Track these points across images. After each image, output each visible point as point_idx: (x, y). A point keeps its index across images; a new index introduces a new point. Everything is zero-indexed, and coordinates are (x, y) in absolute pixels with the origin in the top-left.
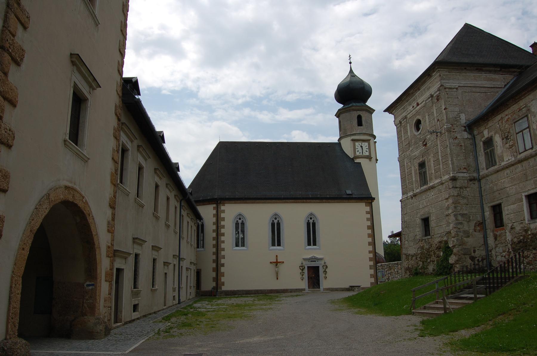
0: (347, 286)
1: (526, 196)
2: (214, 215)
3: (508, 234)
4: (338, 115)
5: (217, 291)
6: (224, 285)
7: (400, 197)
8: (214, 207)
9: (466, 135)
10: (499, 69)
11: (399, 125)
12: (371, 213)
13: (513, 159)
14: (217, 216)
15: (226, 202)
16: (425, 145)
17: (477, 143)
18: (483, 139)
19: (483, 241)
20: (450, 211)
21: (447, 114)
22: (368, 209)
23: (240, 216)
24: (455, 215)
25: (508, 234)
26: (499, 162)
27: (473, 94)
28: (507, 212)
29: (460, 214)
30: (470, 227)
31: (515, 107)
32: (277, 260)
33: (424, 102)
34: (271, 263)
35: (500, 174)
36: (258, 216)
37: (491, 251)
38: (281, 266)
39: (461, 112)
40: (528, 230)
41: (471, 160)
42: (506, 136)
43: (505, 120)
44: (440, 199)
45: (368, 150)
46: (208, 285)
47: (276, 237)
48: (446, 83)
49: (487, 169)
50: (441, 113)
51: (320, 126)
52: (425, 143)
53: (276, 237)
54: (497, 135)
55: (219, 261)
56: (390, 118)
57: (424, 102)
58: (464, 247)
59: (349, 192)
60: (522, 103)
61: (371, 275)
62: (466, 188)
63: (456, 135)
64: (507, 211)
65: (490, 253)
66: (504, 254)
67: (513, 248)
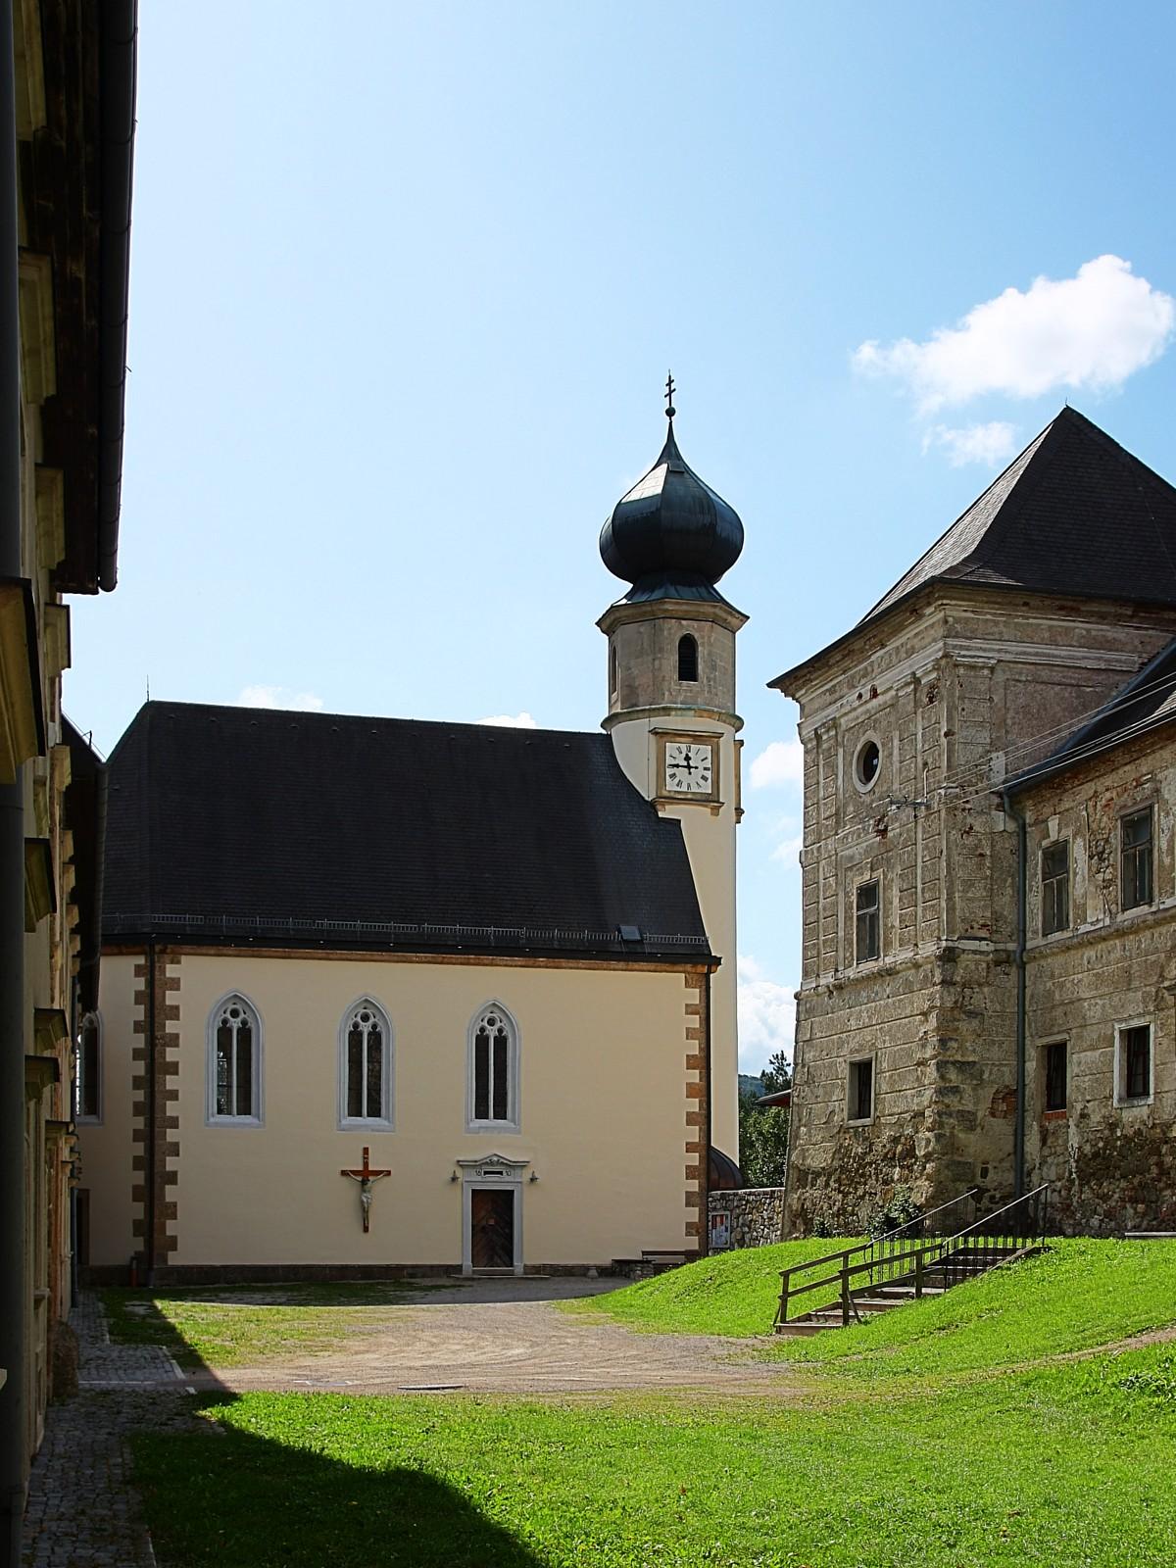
0: (606, 1260)
1: (1121, 1031)
2: (138, 994)
3: (1073, 1130)
4: (610, 623)
5: (150, 1268)
6: (175, 1249)
7: (794, 982)
8: (138, 969)
9: (1001, 821)
10: (1129, 613)
11: (817, 745)
12: (702, 1011)
13: (1107, 922)
14: (150, 999)
15: (187, 948)
16: (883, 833)
17: (1029, 849)
18: (1045, 843)
19: (1012, 1143)
20: (929, 1052)
21: (950, 751)
22: (694, 996)
23: (237, 1005)
24: (940, 1066)
25: (1073, 1130)
26: (1075, 922)
27: (1039, 687)
28: (1076, 1070)
29: (954, 1063)
30: (976, 1101)
31: (1128, 773)
32: (366, 1164)
33: (893, 693)
34: (344, 1173)
35: (1074, 957)
36: (301, 1001)
37: (1029, 1175)
38: (377, 1186)
39: (994, 746)
40: (1117, 1126)
41: (1006, 900)
42: (1100, 849)
43: (1104, 802)
44: (908, 1012)
45: (708, 774)
46: (118, 1246)
47: (366, 1091)
48: (961, 647)
49: (1045, 935)
50: (936, 744)
51: (532, 661)
52: (881, 827)
53: (366, 1091)
54: (1079, 841)
55: (157, 1163)
56: (788, 709)
57: (893, 693)
58: (957, 1158)
59: (630, 932)
60: (1145, 765)
61: (689, 1225)
62: (980, 985)
63: (969, 820)
64: (1078, 1063)
65: (1026, 1180)
66: (1059, 1184)
67: (1079, 1170)
